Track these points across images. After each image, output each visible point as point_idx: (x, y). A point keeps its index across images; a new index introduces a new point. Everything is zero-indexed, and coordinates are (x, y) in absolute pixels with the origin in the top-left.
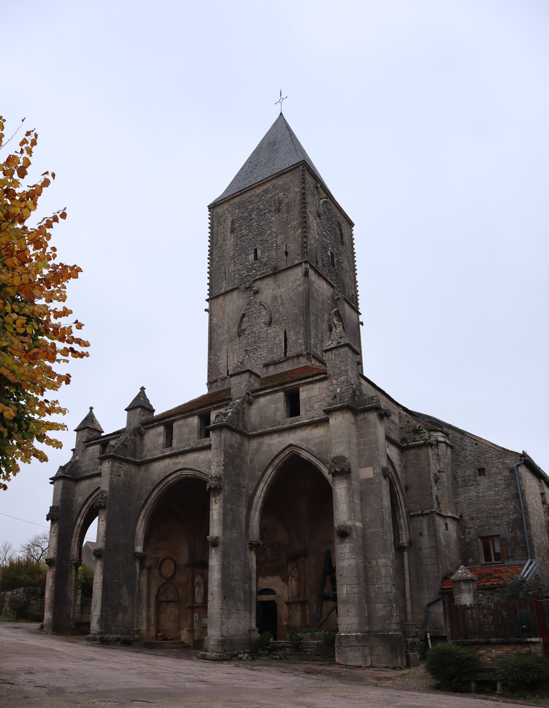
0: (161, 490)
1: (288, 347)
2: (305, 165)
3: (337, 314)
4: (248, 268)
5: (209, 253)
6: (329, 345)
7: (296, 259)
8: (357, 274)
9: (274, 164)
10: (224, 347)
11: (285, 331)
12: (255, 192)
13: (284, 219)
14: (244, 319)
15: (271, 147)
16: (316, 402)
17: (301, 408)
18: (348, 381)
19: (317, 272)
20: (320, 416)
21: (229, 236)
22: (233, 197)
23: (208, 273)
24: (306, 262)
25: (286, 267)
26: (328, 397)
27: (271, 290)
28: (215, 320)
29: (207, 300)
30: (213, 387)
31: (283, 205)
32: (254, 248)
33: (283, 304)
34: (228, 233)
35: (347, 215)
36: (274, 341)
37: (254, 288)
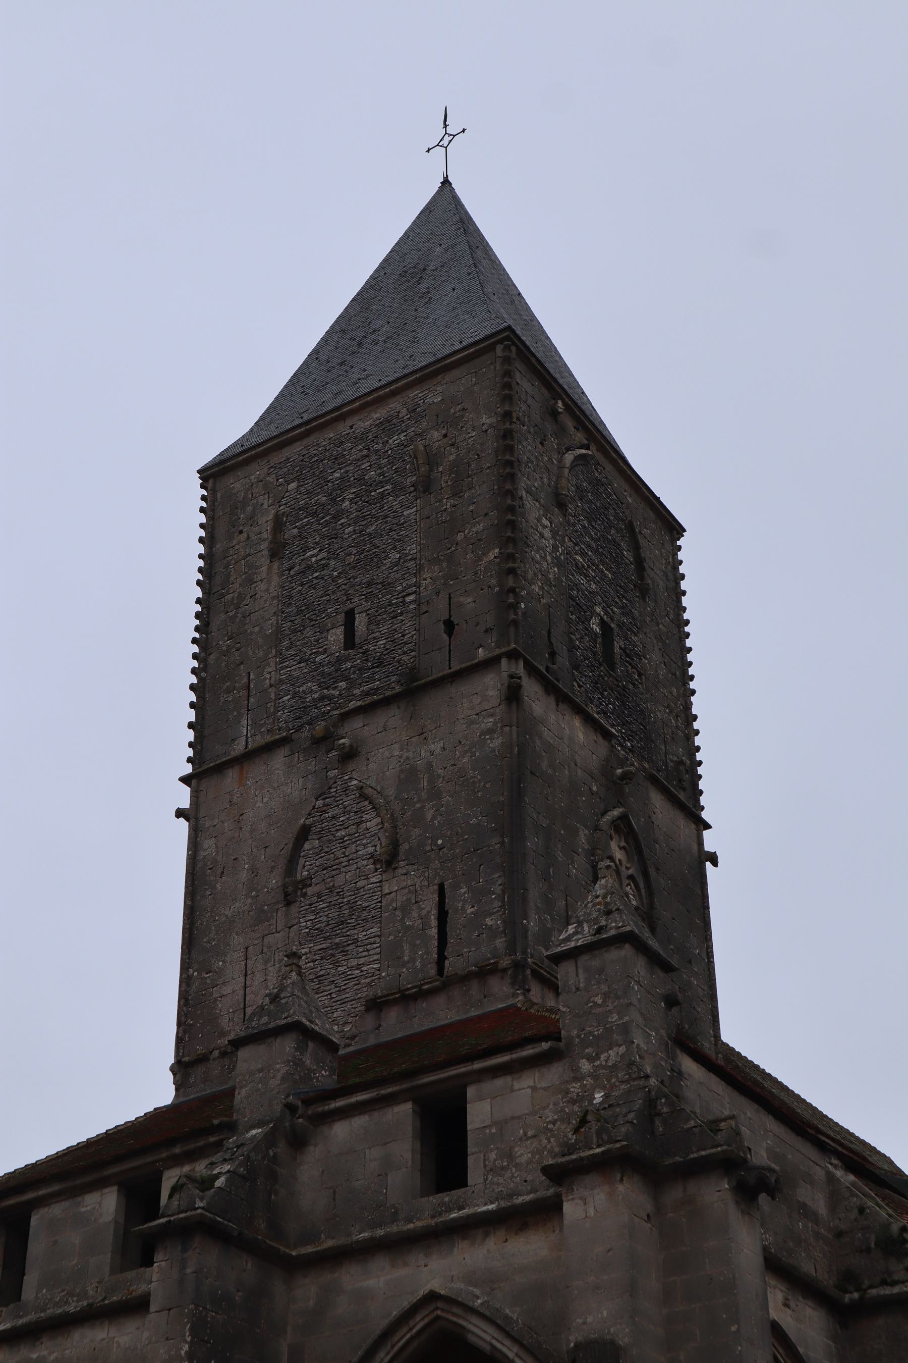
1: (451, 941)
2: (514, 344)
3: (623, 827)
4: (323, 674)
5: (197, 622)
6: (568, 939)
7: (481, 646)
8: (693, 692)
9: (415, 340)
10: (237, 940)
11: (441, 887)
12: (351, 427)
14: (307, 846)
15: (410, 284)
16: (521, 1139)
17: (471, 1161)
18: (632, 1063)
19: (550, 688)
20: (536, 1191)
21: (264, 568)
22: (282, 441)
23: (192, 687)
24: (513, 655)
25: (448, 671)
26: (562, 1120)
27: (397, 746)
28: (208, 845)
29: (185, 780)
30: (192, 1081)
31: (441, 469)
32: (346, 609)
33: (435, 794)
34: (263, 560)
35: (658, 499)
36: (403, 919)
37: (341, 741)
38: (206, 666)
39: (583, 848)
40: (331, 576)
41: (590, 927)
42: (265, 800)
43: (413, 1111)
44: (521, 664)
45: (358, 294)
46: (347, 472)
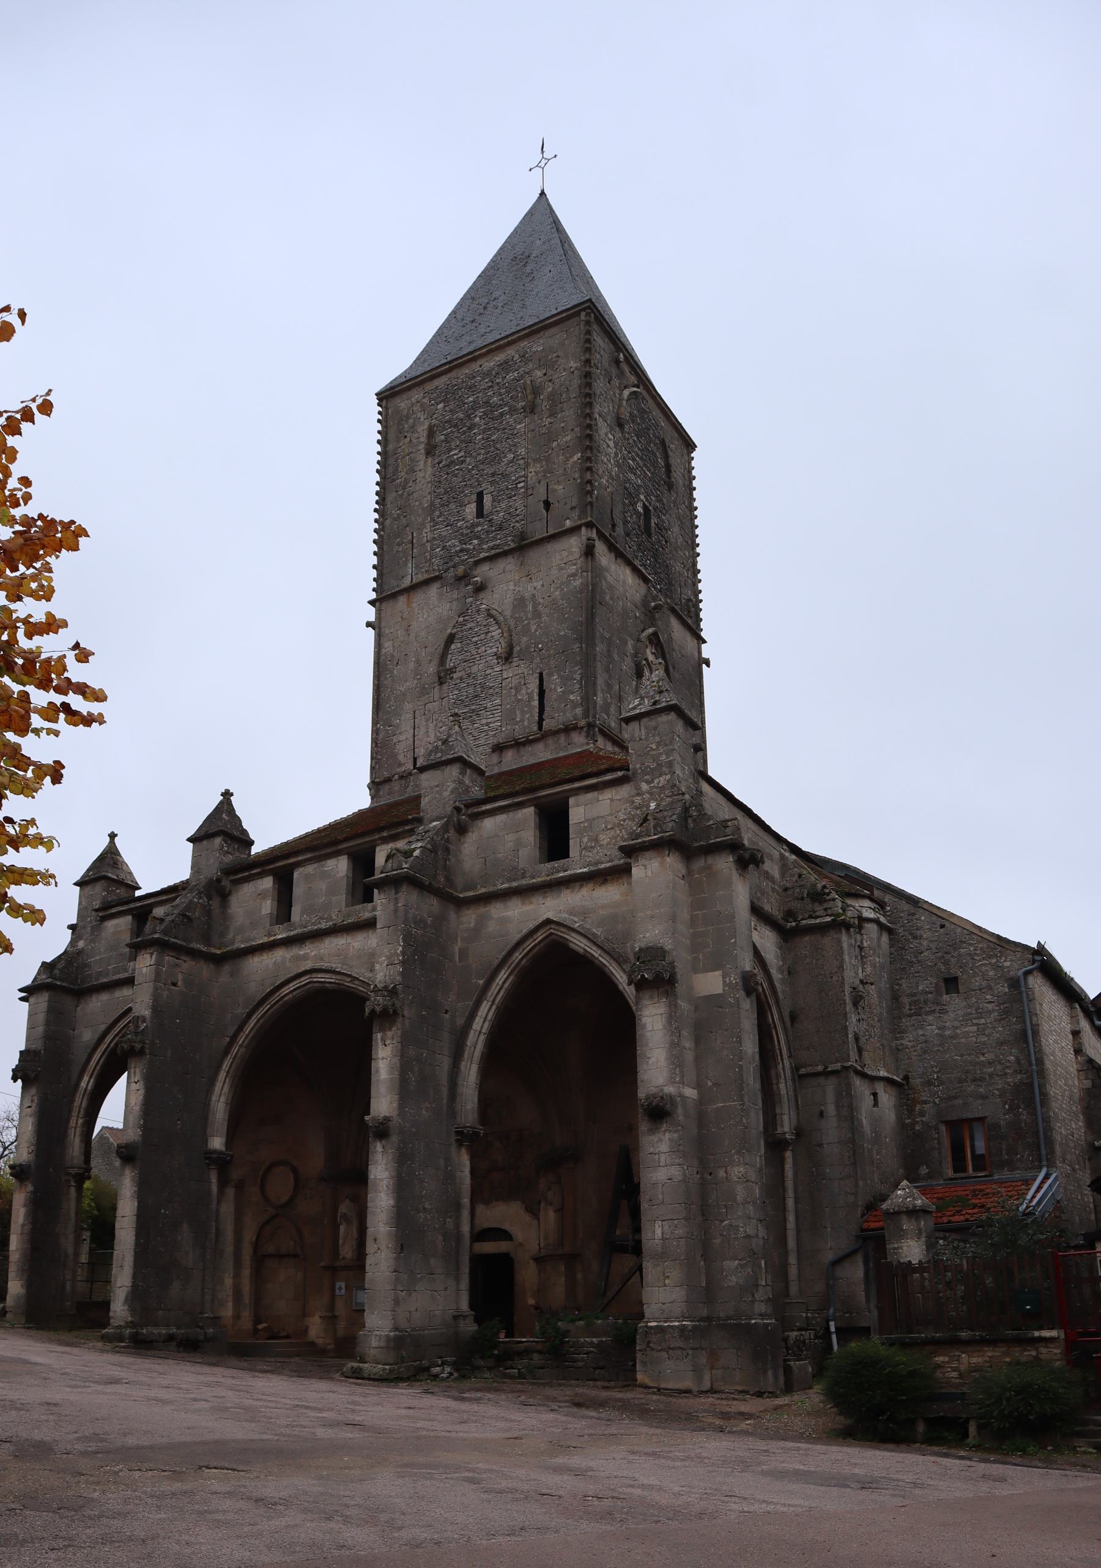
0: (266, 1016)
1: (547, 709)
2: (593, 312)
3: (655, 640)
4: (462, 534)
5: (377, 498)
6: (635, 708)
7: (568, 518)
8: (698, 555)
10: (408, 706)
11: (541, 675)
12: (481, 366)
14: (453, 647)
16: (603, 830)
17: (571, 842)
18: (674, 785)
19: (612, 548)
21: (422, 462)
22: (433, 375)
23: (375, 542)
24: (589, 525)
25: (546, 535)
26: (629, 819)
28: (388, 646)
29: (372, 603)
30: (381, 793)
31: (542, 397)
32: (478, 491)
33: (537, 615)
34: (421, 456)
35: (680, 424)
36: (516, 694)
38: (383, 528)
39: (630, 653)
40: (467, 468)
41: (649, 701)
42: (425, 617)
43: (535, 812)
44: (595, 531)
45: (482, 272)
46: (477, 397)
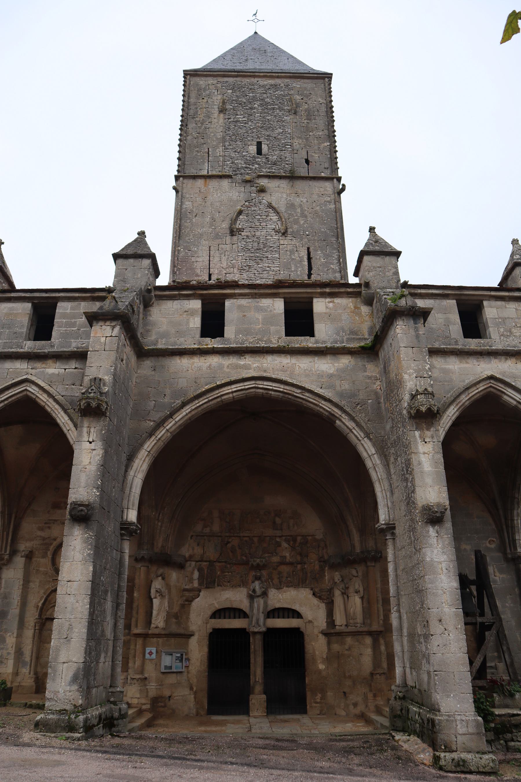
0: (200, 409)
4: (247, 160)
11: (308, 249)
13: (304, 124)
14: (241, 217)
28: (188, 205)
42: (218, 195)
